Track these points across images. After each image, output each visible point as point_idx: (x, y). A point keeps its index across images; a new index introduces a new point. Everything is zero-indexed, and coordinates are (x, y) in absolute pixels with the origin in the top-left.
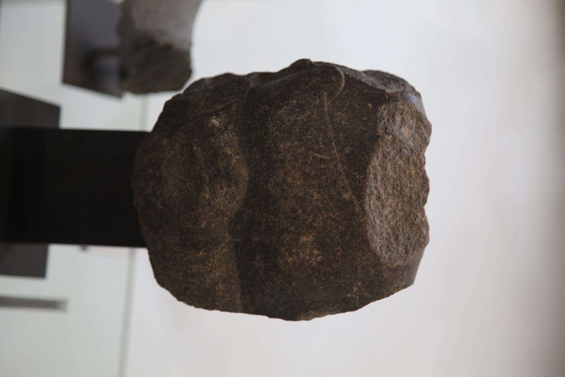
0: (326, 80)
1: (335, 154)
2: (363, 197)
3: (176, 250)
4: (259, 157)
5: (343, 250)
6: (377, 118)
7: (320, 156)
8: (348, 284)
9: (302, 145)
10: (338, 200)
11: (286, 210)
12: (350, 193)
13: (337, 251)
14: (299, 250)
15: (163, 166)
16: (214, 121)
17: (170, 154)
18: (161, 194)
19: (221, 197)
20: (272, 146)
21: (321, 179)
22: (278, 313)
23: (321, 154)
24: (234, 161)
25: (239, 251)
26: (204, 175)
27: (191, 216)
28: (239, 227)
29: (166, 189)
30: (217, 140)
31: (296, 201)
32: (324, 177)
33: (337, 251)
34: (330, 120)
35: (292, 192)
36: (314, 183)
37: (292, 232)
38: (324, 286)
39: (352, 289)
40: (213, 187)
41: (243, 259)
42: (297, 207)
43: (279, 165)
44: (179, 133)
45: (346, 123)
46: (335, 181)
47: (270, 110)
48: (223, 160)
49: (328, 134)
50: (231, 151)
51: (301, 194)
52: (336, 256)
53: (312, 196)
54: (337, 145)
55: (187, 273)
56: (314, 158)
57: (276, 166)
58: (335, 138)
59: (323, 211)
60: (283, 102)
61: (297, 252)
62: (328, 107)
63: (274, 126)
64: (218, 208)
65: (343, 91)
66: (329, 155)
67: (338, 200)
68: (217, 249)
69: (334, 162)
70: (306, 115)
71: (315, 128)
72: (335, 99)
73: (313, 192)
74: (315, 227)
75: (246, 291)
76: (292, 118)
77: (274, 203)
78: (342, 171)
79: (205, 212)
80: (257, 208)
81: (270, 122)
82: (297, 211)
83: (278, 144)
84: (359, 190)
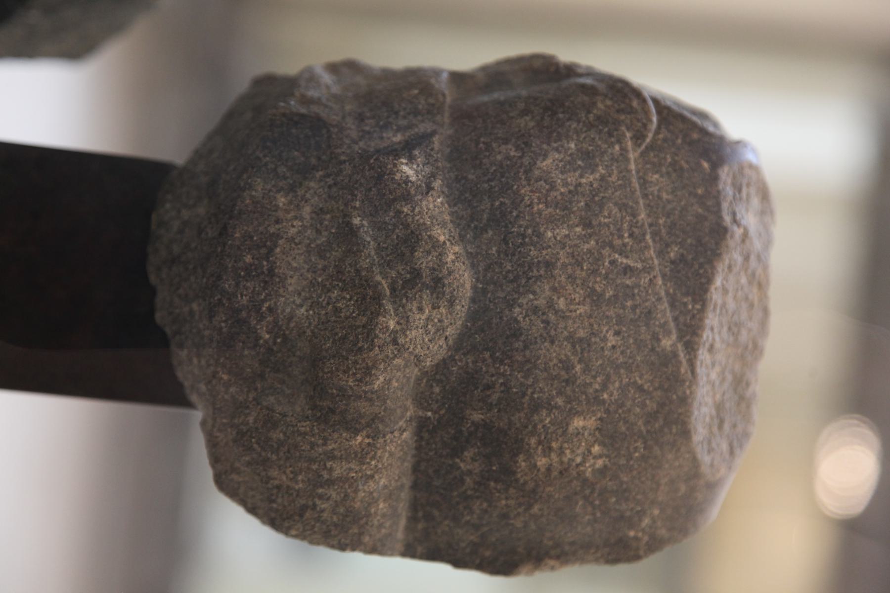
0: (623, 106)
1: (652, 258)
2: (696, 347)
4: (498, 252)
5: (645, 448)
7: (625, 261)
8: (638, 512)
9: (590, 236)
10: (653, 350)
11: (551, 364)
12: (674, 337)
14: (566, 445)
15: (278, 250)
16: (405, 168)
17: (293, 226)
18: (270, 309)
20: (530, 231)
21: (624, 307)
22: (478, 561)
23: (627, 257)
25: (426, 435)
26: (378, 278)
27: (356, 362)
28: (437, 390)
29: (283, 299)
30: (417, 210)
31: (574, 347)
32: (629, 303)
33: (636, 449)
34: (641, 188)
35: (566, 328)
37: (557, 407)
38: (594, 514)
39: (640, 520)
40: (403, 307)
41: (431, 453)
42: (574, 359)
43: (542, 272)
44: (312, 184)
45: (670, 197)
46: (650, 312)
47: (520, 158)
48: (429, 253)
51: (581, 334)
52: (631, 458)
53: (605, 339)
54: (654, 241)
55: (320, 476)
56: (613, 262)
58: (651, 225)
59: (622, 371)
60: (549, 145)
61: (561, 448)
62: (635, 161)
63: (531, 191)
67: (653, 350)
68: (392, 433)
69: (649, 273)
70: (597, 176)
71: (616, 204)
72: (647, 148)
73: (607, 332)
74: (604, 401)
75: (420, 514)
76: (572, 178)
77: (526, 347)
78: (663, 293)
79: (387, 357)
80: (487, 355)
81: (524, 183)
83: (542, 230)
84: (690, 332)
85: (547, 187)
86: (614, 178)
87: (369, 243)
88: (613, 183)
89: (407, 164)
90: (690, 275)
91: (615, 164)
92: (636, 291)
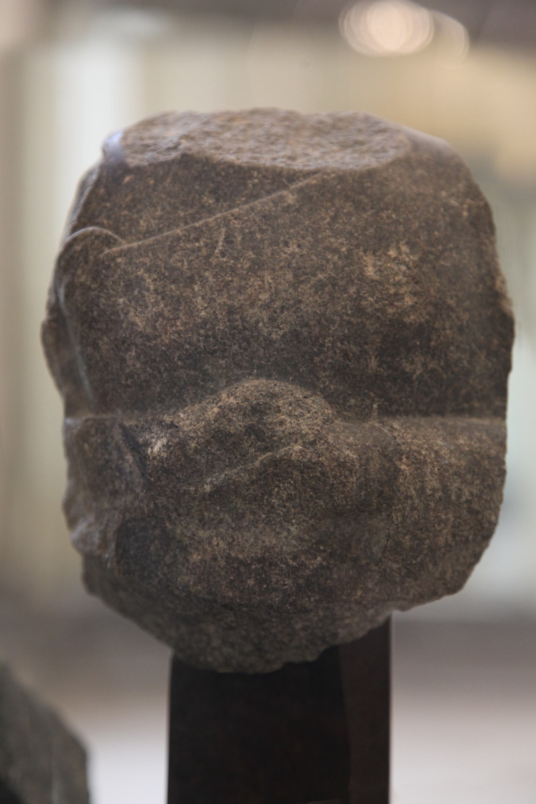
0: (81, 259)
2: (292, 172)
3: (400, 519)
4: (223, 358)
5: (387, 209)
7: (221, 243)
8: (445, 210)
9: (201, 276)
10: (298, 211)
11: (320, 301)
13: (389, 217)
14: (391, 281)
15: (240, 556)
16: (156, 449)
17: (218, 545)
18: (294, 558)
19: (298, 424)
20: (202, 332)
21: (262, 240)
22: (504, 350)
23: (217, 242)
24: (232, 400)
25: (395, 407)
26: (257, 463)
27: (335, 477)
28: (352, 401)
30: (192, 435)
31: (302, 282)
34: (154, 235)
35: (286, 291)
36: (268, 251)
37: (358, 292)
39: (453, 207)
41: (410, 401)
42: (313, 280)
43: (238, 317)
44: (178, 531)
45: (159, 208)
47: (136, 346)
48: (230, 420)
51: (290, 276)
53: (293, 255)
54: (200, 219)
56: (223, 254)
57: (239, 323)
58: (186, 223)
59: (320, 236)
61: (394, 285)
62: (129, 242)
63: (166, 333)
64: (319, 428)
67: (298, 211)
68: (395, 438)
69: (229, 221)
70: (146, 275)
71: (170, 256)
73: (286, 253)
74: (349, 250)
76: (151, 298)
79: (327, 449)
80: (317, 359)
81: (159, 340)
82: (320, 281)
83: (200, 321)
84: (279, 178)
85: (161, 320)
86: (147, 261)
87: (226, 475)
88: (151, 260)
89: (152, 448)
91: (134, 260)
92: (247, 231)
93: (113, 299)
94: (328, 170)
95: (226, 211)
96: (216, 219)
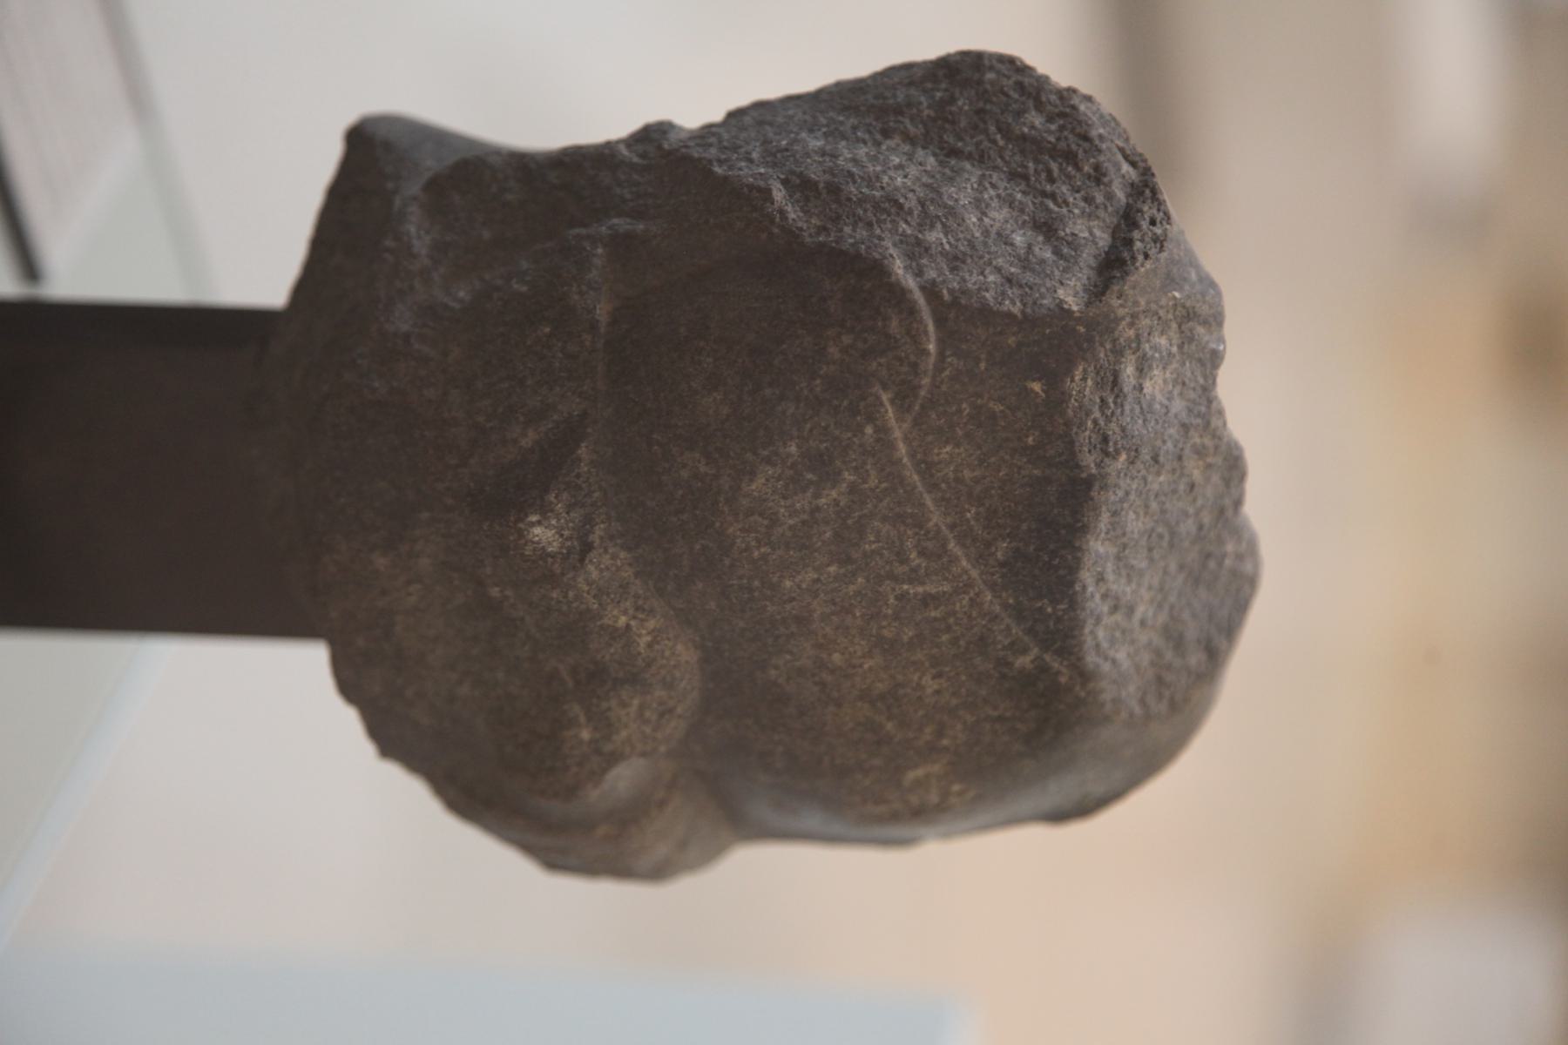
6: (1068, 424)
7: (920, 589)
9: (854, 574)
23: (923, 583)
30: (571, 594)
36: (919, 656)
49: (931, 524)
50: (625, 612)
53: (919, 687)
54: (964, 546)
56: (901, 597)
59: (961, 713)
65: (939, 369)
66: (946, 579)
71: (884, 519)
72: (923, 407)
76: (802, 502)
78: (997, 609)
85: (766, 522)
86: (873, 481)
87: (522, 619)
88: (872, 490)
89: (539, 523)
90: (1037, 572)
91: (870, 460)
92: (951, 620)
93: (795, 433)
94: (1215, 422)
95: (984, 582)
96: (966, 572)
